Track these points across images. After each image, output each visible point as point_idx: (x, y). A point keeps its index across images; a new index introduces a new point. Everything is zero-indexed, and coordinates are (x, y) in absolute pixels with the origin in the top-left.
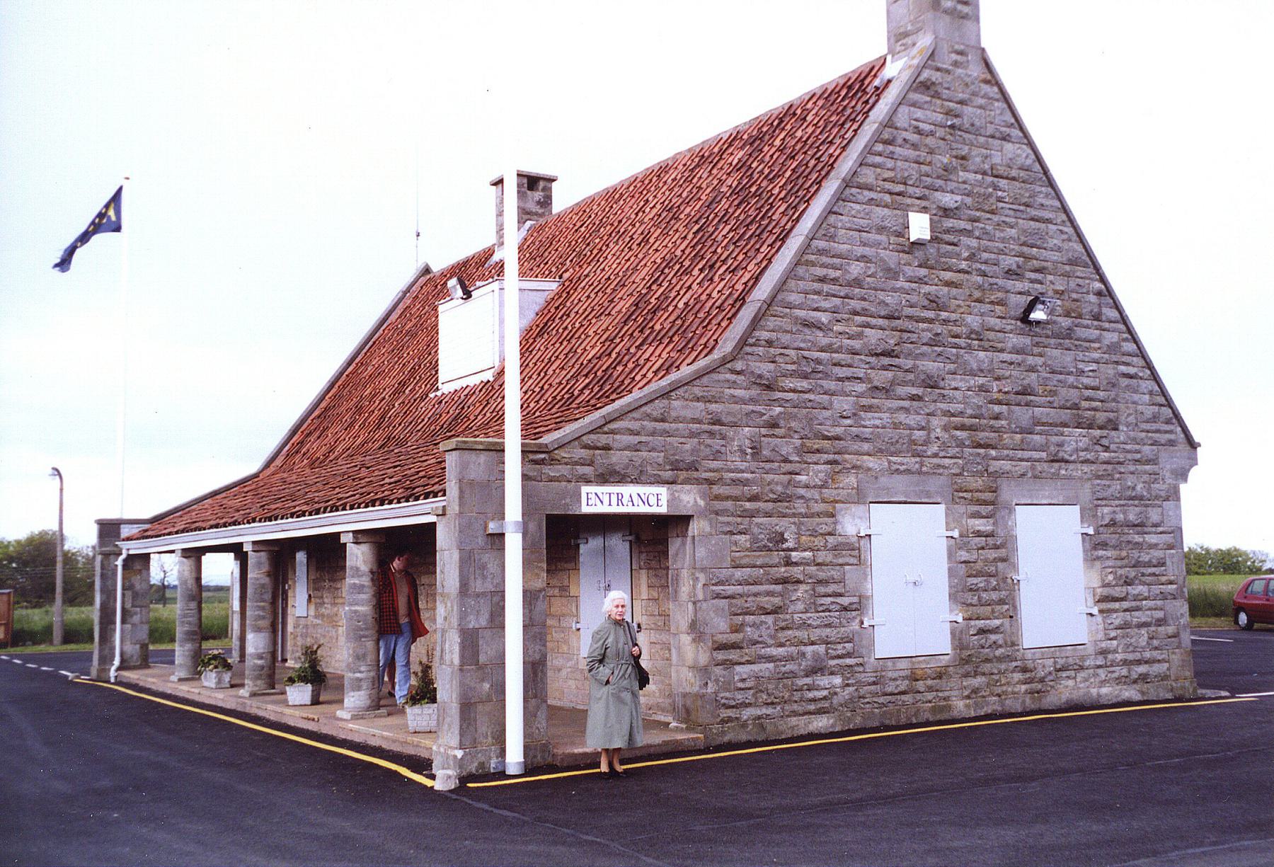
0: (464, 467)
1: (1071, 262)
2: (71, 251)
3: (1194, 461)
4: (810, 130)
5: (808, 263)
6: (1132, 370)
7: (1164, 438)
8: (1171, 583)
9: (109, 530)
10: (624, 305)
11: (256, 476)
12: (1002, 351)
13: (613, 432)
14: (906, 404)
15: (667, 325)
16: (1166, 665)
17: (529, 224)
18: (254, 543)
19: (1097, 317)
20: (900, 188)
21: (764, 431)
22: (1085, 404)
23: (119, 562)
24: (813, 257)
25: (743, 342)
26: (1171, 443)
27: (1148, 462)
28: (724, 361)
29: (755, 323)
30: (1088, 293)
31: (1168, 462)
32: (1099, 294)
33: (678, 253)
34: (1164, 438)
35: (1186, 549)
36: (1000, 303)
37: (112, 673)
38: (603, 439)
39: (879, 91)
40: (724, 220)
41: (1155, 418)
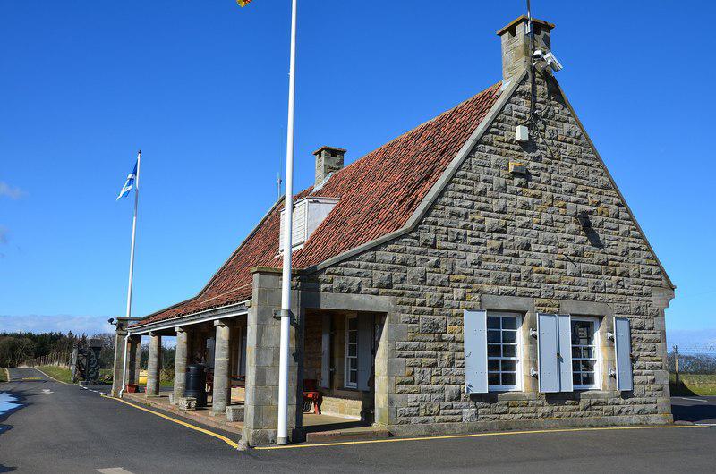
0: (261, 282)
1: (603, 187)
2: (558, 355)
3: (672, 296)
4: (463, 118)
5: (456, 182)
6: (636, 246)
7: (656, 282)
8: (659, 361)
9: (122, 324)
10: (367, 208)
11: (195, 299)
12: (563, 232)
13: (346, 266)
14: (509, 258)
15: (385, 216)
16: (654, 406)
17: (331, 174)
18: (180, 327)
19: (617, 217)
20: (506, 145)
21: (428, 269)
22: (610, 263)
23: (126, 339)
24: (457, 179)
25: (419, 222)
26: (661, 286)
27: (647, 295)
28: (407, 234)
29: (427, 213)
30: (612, 204)
31: (656, 299)
32: (618, 204)
33: (395, 181)
34: (656, 282)
35: (670, 350)
36: (564, 207)
37: (121, 393)
38: (338, 270)
39: (497, 97)
40: (418, 164)
41: (649, 272)
